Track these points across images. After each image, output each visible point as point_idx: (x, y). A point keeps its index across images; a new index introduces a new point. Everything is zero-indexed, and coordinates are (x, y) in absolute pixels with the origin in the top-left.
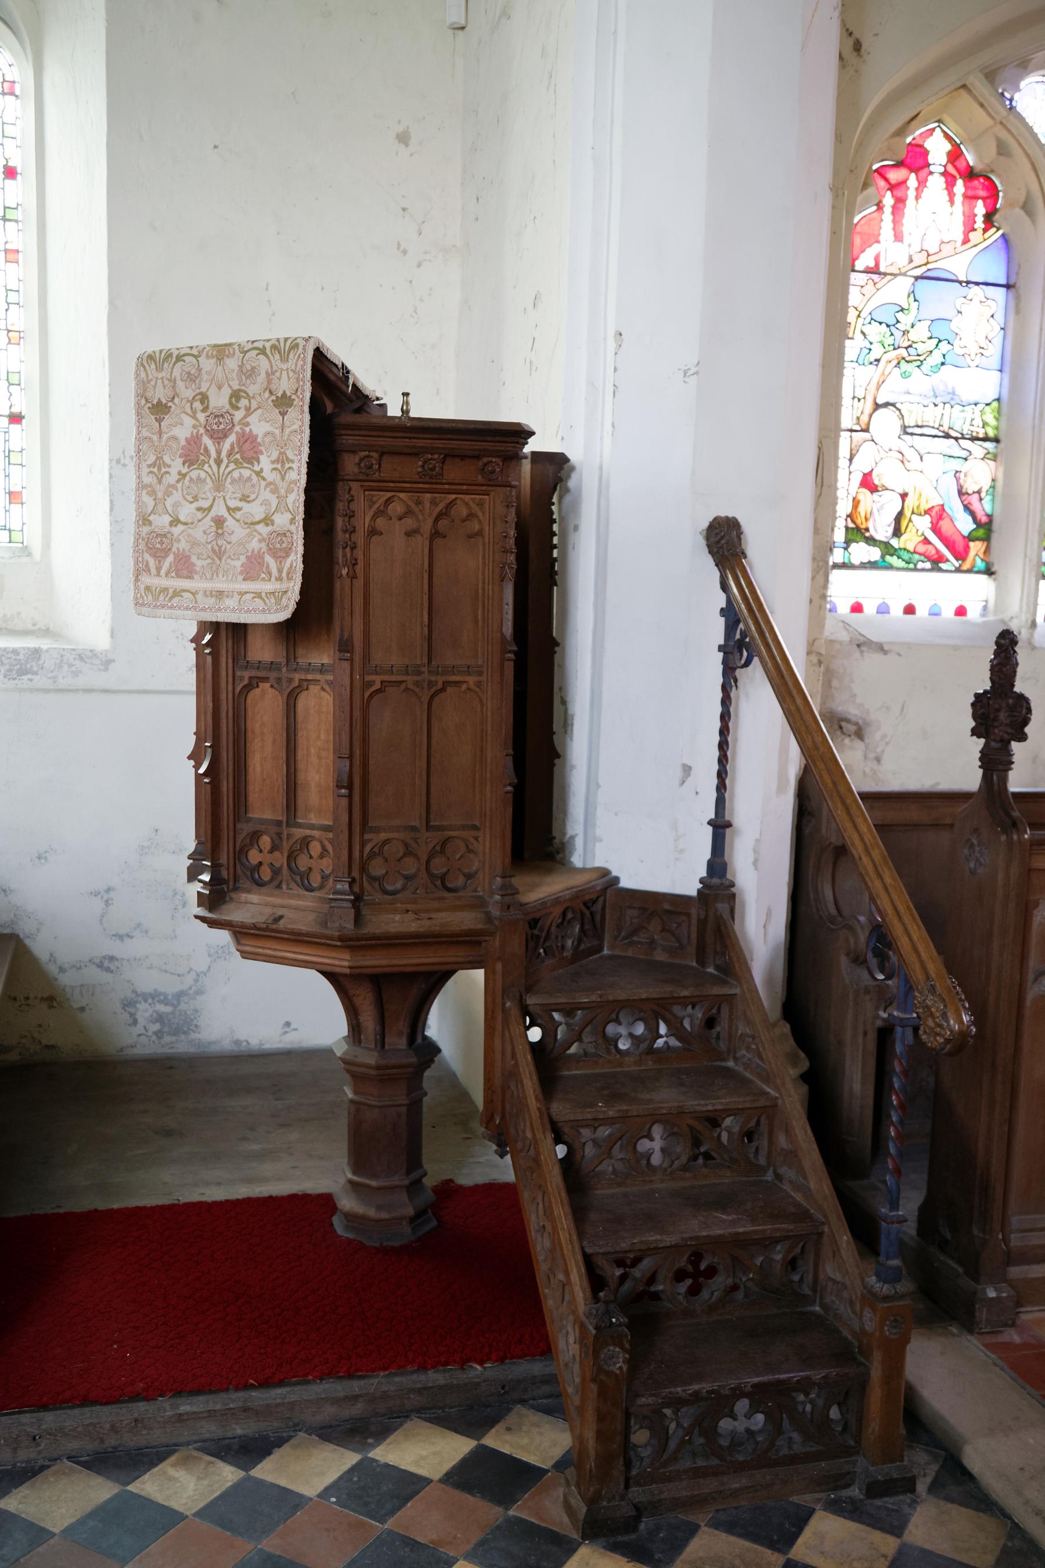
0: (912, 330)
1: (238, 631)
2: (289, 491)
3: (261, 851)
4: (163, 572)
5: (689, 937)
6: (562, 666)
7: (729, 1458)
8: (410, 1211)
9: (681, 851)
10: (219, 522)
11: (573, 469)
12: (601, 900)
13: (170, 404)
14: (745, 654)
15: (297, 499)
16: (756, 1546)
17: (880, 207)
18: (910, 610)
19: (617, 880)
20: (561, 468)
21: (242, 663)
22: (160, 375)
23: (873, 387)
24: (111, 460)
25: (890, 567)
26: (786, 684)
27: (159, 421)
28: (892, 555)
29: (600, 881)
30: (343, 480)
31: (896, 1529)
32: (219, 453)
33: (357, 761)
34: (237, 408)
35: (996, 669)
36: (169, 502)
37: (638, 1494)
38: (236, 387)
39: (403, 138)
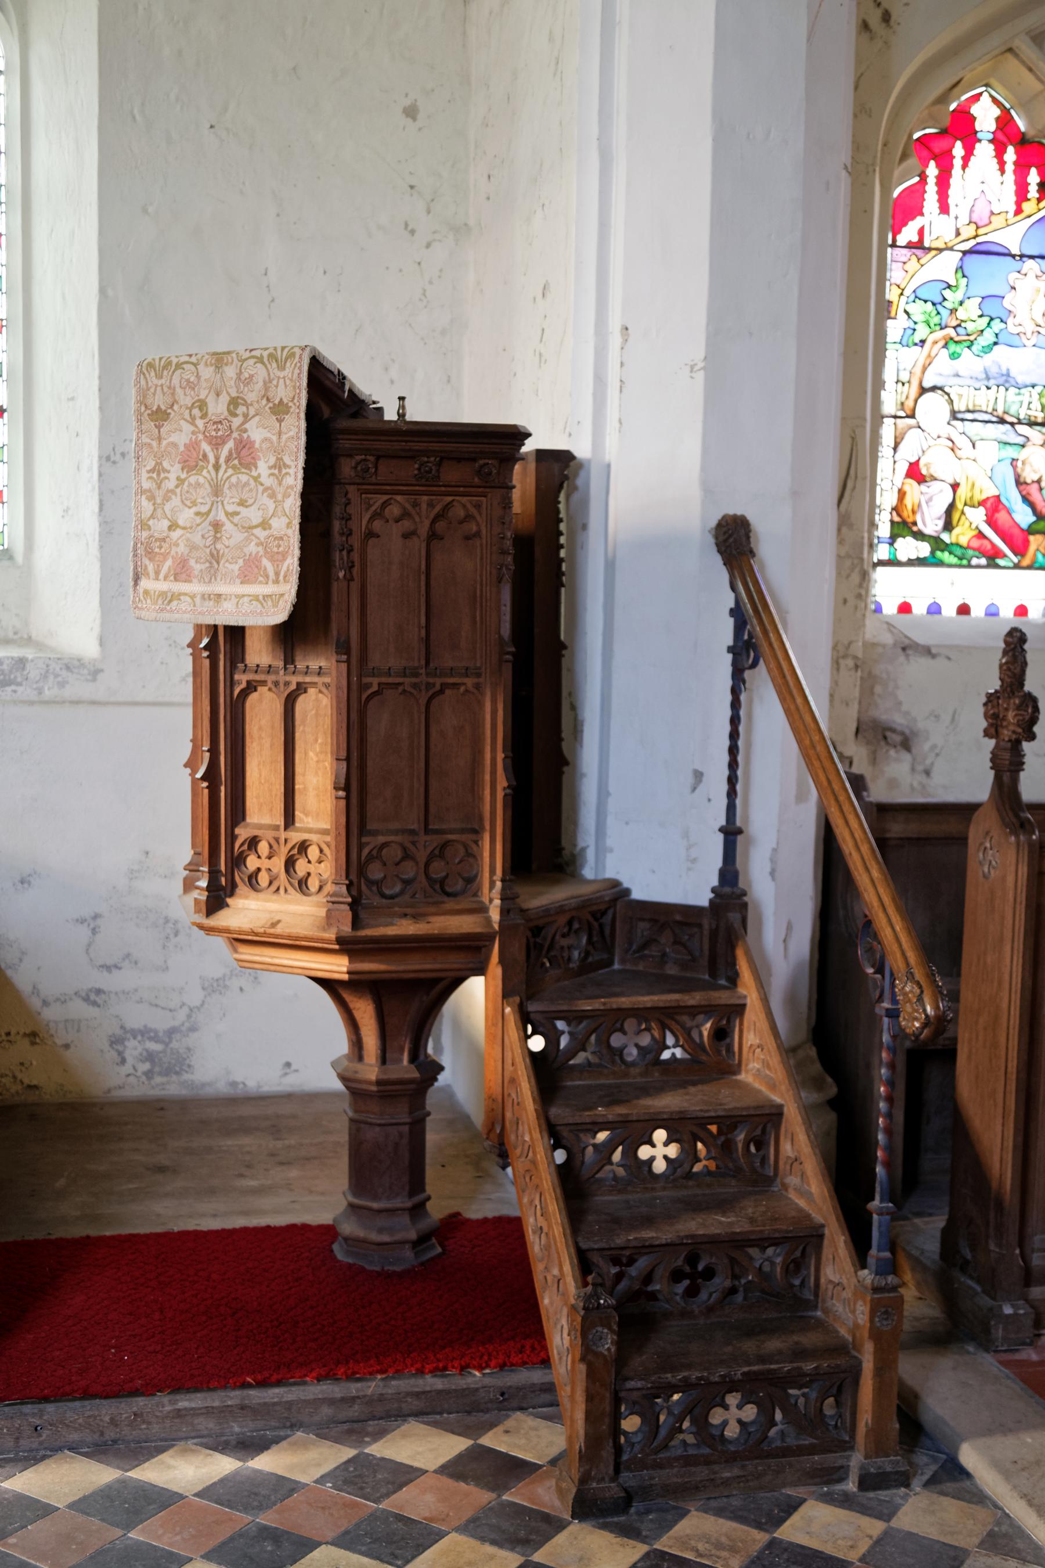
0: (960, 309)
1: (236, 634)
2: (286, 496)
3: (259, 857)
4: (161, 576)
5: (702, 951)
6: (571, 670)
7: (720, 1448)
8: (413, 1235)
9: (694, 861)
10: (217, 526)
11: (580, 465)
12: (610, 912)
13: (169, 411)
14: (752, 654)
15: (293, 504)
16: (742, 1527)
17: (923, 177)
18: (964, 610)
19: (627, 892)
20: (567, 466)
21: (241, 666)
22: (160, 382)
23: (918, 370)
24: (100, 458)
25: (941, 564)
26: (787, 683)
27: (159, 427)
28: (942, 551)
29: (609, 892)
30: (340, 483)
31: (886, 1514)
32: (217, 459)
33: (355, 762)
34: (236, 415)
35: (1005, 667)
36: (168, 507)
37: (628, 1478)
38: (234, 394)
39: (411, 112)
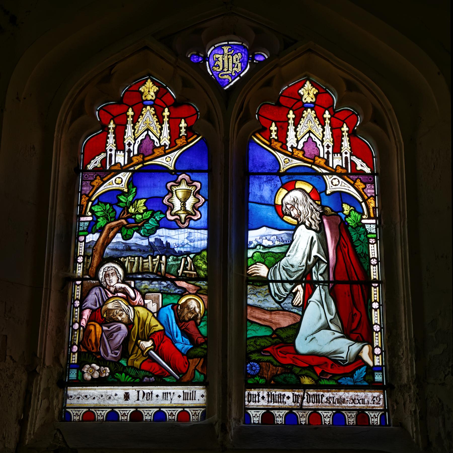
28: (121, 373)
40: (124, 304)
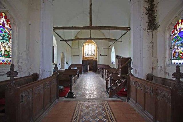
40: (178, 50)
